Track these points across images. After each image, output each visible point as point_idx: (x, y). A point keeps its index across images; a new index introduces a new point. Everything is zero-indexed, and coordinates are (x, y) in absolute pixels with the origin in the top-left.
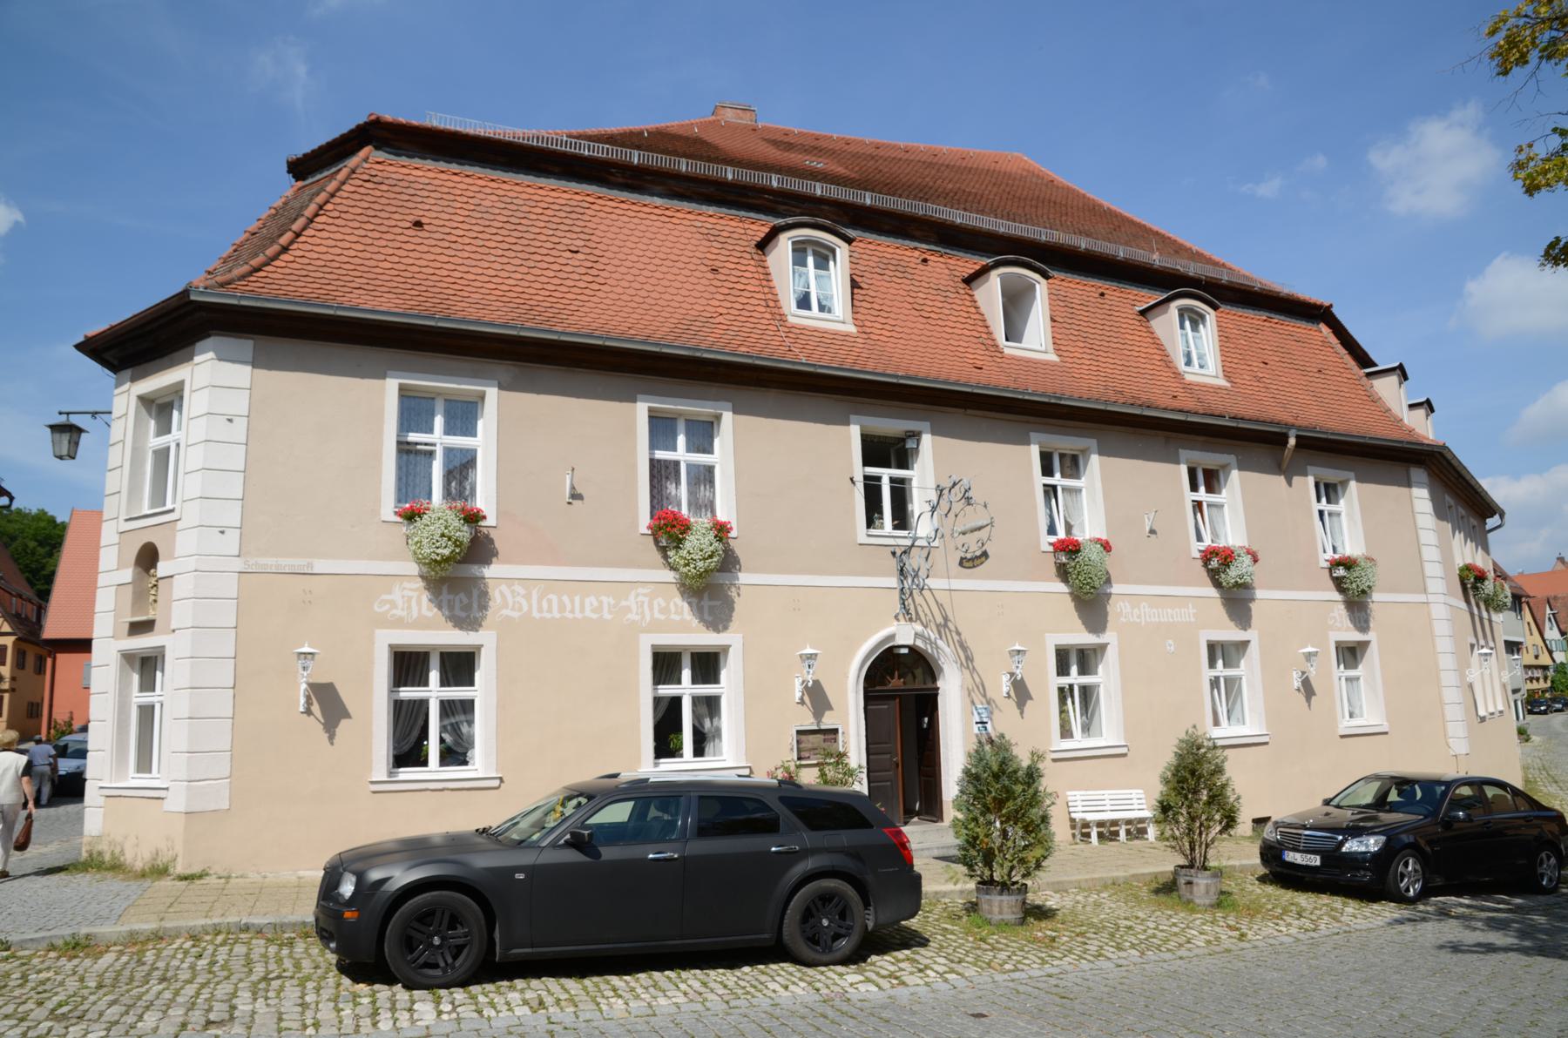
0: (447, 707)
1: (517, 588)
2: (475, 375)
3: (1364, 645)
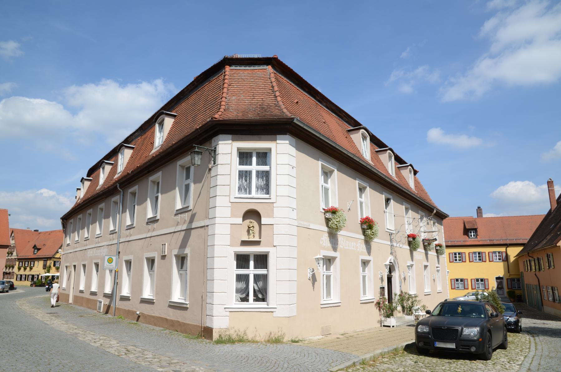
0: (257, 278)
2: (333, 164)
3: (334, 258)
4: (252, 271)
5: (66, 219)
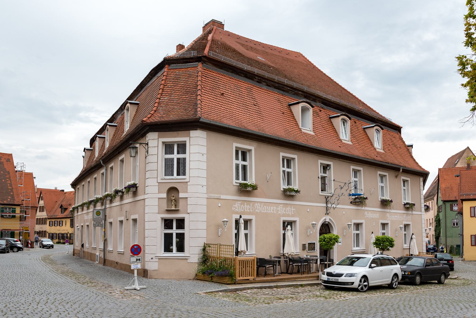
1: (259, 204)
4: (174, 231)
5: (75, 185)
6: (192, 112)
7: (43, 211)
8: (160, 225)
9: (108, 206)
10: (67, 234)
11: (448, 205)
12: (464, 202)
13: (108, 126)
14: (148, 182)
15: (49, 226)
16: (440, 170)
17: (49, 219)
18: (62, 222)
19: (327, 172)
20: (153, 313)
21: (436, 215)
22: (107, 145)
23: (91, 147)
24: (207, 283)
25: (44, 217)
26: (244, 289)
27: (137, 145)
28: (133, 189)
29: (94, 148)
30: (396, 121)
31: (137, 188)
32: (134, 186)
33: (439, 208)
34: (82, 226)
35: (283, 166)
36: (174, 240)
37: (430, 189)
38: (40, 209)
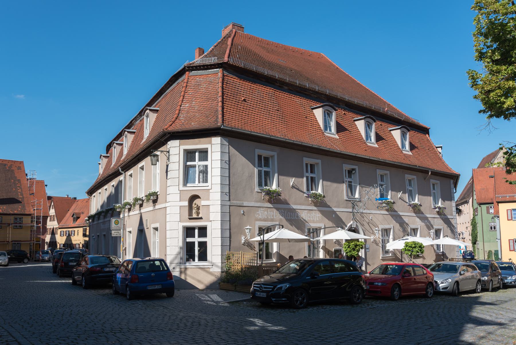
6: (213, 119)
7: (54, 220)
8: (180, 234)
9: (126, 215)
10: (79, 245)
11: (484, 207)
12: (499, 204)
13: (126, 132)
14: (170, 190)
15: (61, 236)
16: (473, 170)
17: (60, 228)
18: (74, 231)
19: (352, 176)
20: (178, 322)
21: (472, 218)
22: (125, 152)
23: (107, 153)
24: (231, 293)
25: (55, 227)
26: (262, 134)
27: (158, 153)
28: (154, 198)
29: (111, 154)
30: (423, 123)
31: (157, 196)
32: (155, 194)
33: (475, 210)
34: (98, 236)
35: (307, 172)
36: (197, 248)
37: (464, 193)
38: (50, 218)
